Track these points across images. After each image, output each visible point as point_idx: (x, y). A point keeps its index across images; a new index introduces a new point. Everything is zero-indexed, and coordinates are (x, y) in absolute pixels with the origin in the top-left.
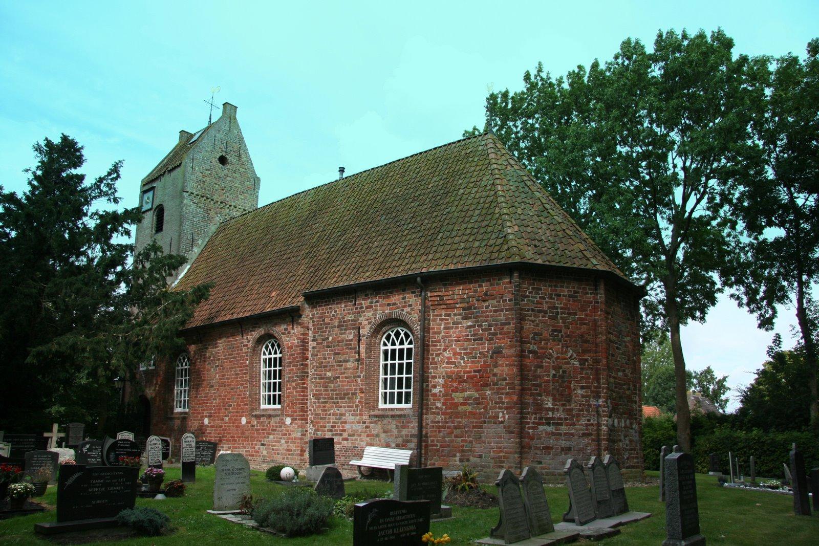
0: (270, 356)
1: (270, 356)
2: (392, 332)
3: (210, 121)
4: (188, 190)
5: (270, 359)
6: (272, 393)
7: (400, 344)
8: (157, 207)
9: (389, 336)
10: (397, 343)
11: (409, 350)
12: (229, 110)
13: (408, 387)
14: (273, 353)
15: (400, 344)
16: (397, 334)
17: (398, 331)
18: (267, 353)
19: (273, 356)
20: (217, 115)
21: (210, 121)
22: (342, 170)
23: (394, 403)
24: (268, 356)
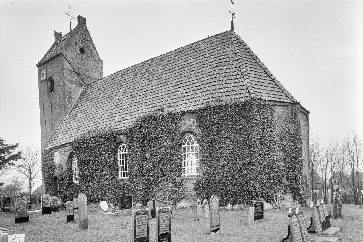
0: (123, 153)
1: (123, 153)
2: (187, 138)
3: (71, 28)
4: (66, 68)
5: (123, 154)
6: (125, 171)
7: (125, 151)
8: (49, 78)
9: (121, 148)
10: (190, 144)
11: (126, 154)
12: (81, 20)
13: (126, 170)
14: (124, 151)
15: (125, 151)
16: (190, 138)
17: (190, 137)
18: (121, 152)
19: (124, 153)
20: (75, 24)
21: (71, 28)
22: (208, 36)
23: (124, 177)
24: (121, 153)
